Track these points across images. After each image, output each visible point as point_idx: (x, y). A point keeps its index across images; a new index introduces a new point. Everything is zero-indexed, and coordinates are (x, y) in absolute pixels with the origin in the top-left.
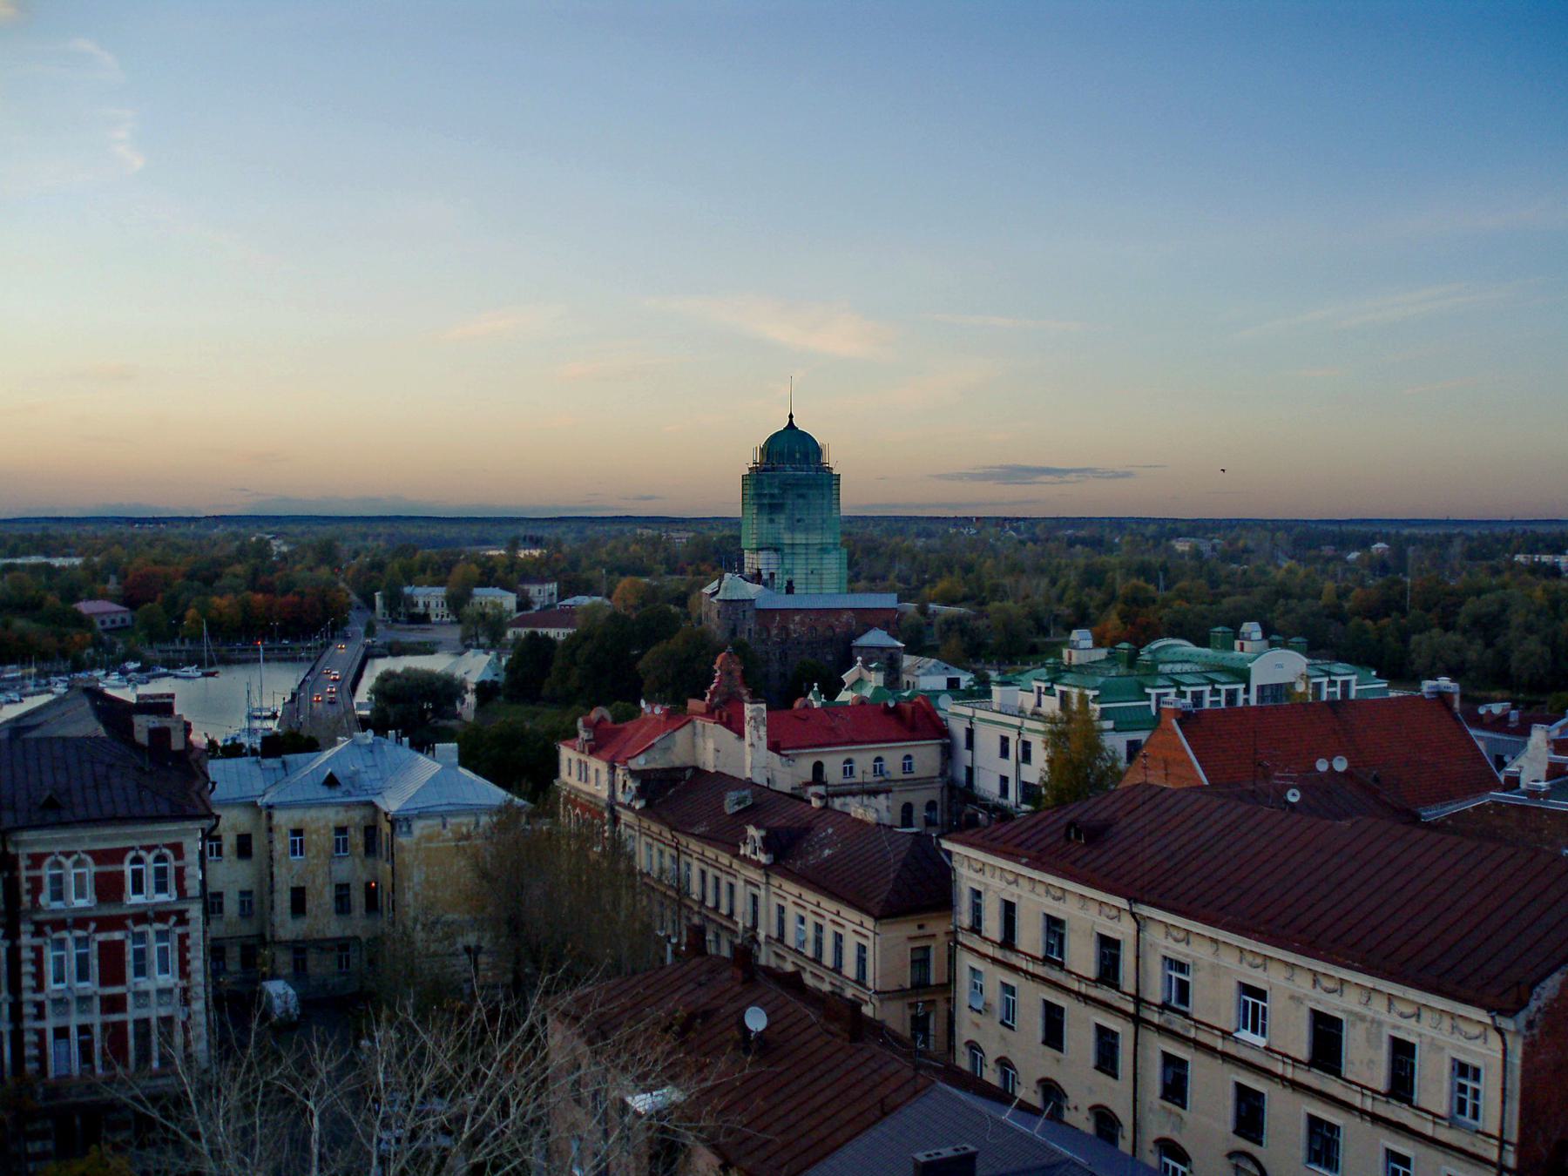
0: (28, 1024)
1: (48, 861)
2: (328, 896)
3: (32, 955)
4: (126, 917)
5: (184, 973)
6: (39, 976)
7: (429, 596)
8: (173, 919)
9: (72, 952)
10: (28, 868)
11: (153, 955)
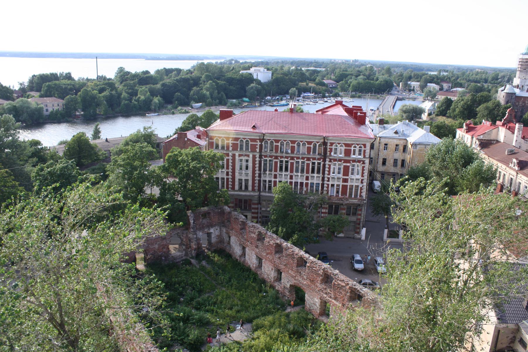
0: (326, 182)
1: (334, 145)
2: (392, 161)
3: (328, 166)
4: (351, 160)
5: (362, 176)
6: (329, 171)
7: (414, 84)
8: (362, 162)
9: (337, 167)
10: (329, 146)
11: (356, 170)
